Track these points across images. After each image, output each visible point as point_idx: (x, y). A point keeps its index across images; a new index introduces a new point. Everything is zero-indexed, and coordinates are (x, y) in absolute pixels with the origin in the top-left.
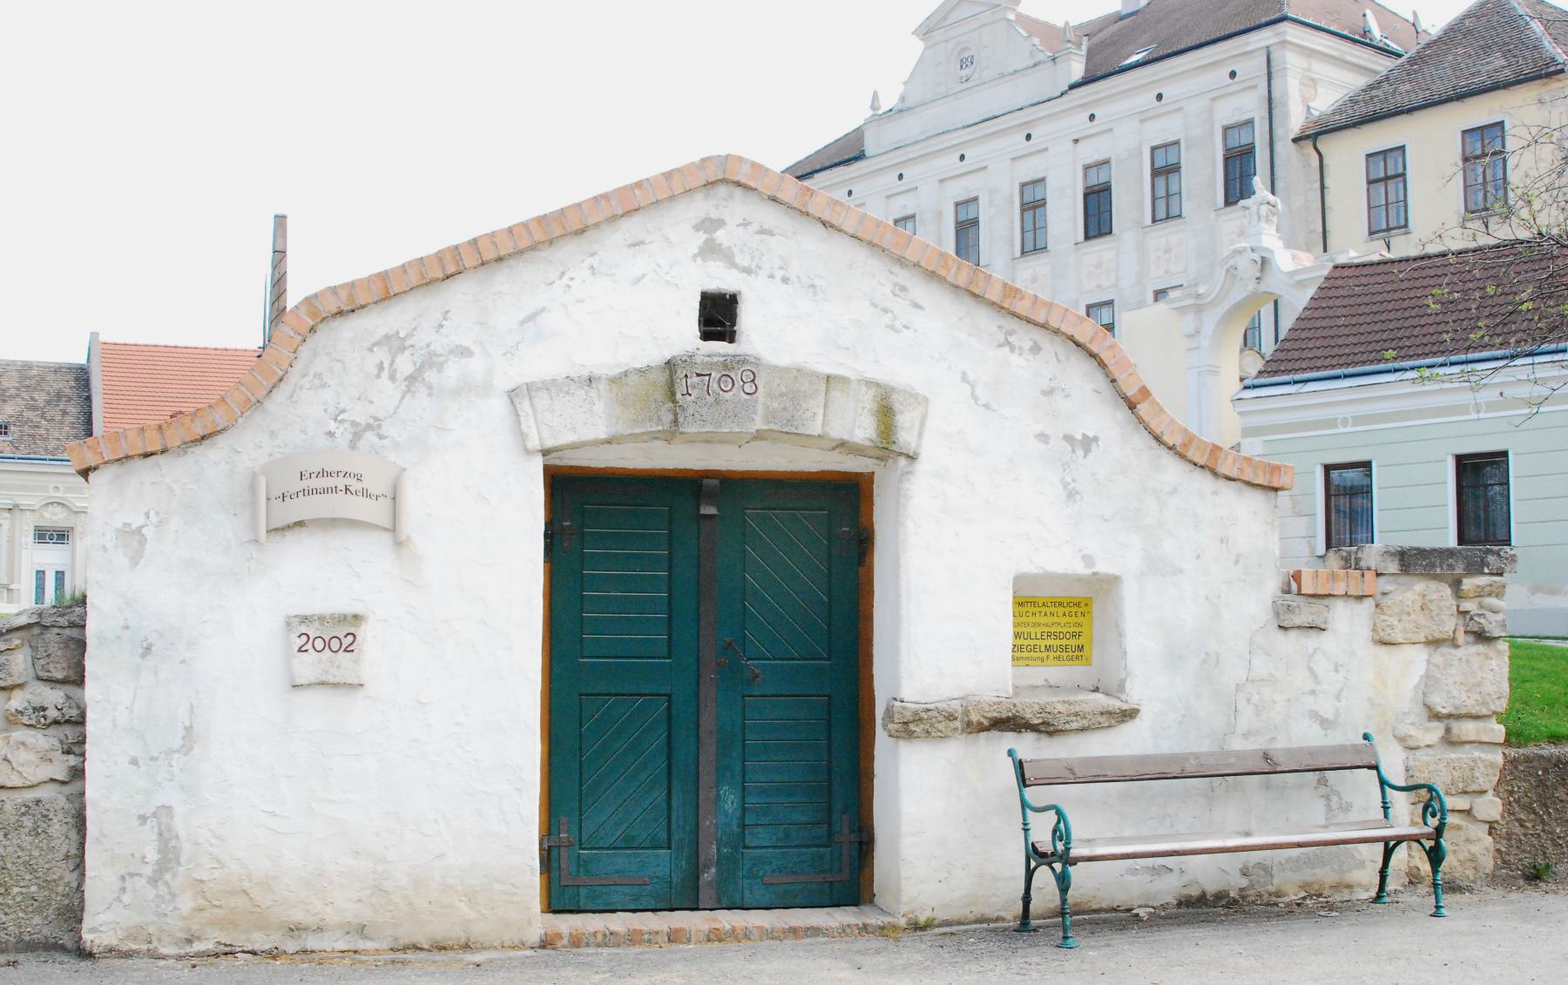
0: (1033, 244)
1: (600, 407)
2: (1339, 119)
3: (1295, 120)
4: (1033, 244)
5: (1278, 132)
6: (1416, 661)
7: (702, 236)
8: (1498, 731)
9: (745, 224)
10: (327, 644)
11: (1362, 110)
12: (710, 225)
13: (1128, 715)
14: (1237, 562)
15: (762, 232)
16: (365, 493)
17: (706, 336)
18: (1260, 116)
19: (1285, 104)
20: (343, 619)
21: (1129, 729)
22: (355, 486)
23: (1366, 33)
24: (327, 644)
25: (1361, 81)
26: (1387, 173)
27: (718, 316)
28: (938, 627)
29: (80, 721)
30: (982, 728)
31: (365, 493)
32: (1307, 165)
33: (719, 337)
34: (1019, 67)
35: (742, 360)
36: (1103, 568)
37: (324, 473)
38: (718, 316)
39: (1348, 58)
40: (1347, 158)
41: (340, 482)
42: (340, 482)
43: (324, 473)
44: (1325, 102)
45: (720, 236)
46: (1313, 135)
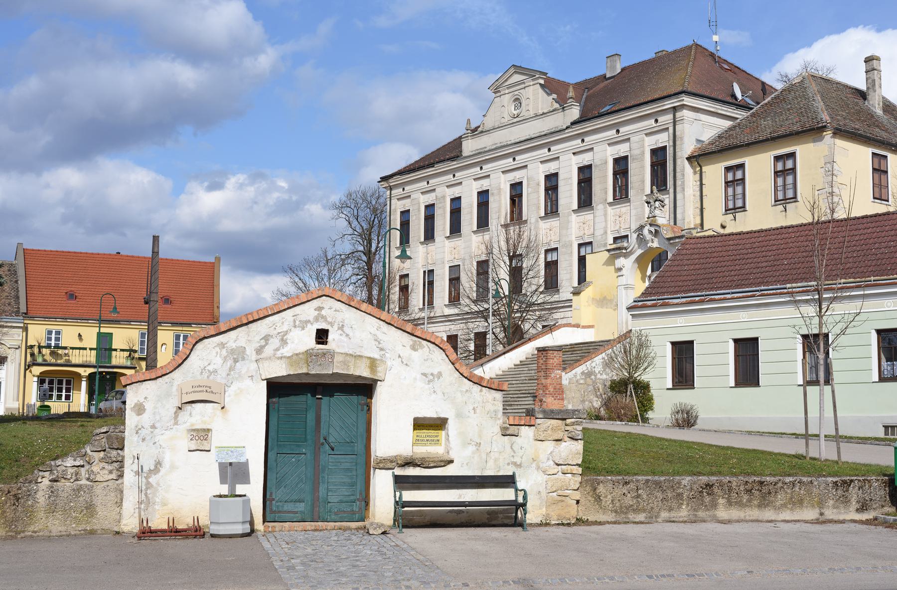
0: (552, 209)
1: (284, 366)
2: (714, 148)
3: (688, 147)
4: (552, 209)
5: (678, 154)
6: (549, 446)
7: (317, 312)
8: (580, 470)
9: (330, 308)
10: (199, 438)
11: (725, 143)
12: (320, 309)
13: (451, 462)
14: (420, 424)
15: (336, 311)
16: (212, 392)
17: (318, 343)
18: (669, 145)
19: (682, 138)
20: (204, 430)
21: (451, 466)
22: (209, 390)
23: (734, 96)
24: (199, 438)
25: (728, 124)
26: (735, 180)
27: (322, 336)
28: (391, 432)
29: (122, 462)
30: (403, 466)
31: (212, 392)
32: (695, 173)
33: (322, 343)
34: (545, 111)
35: (329, 351)
36: (442, 416)
37: (199, 386)
38: (322, 336)
39: (720, 112)
40: (715, 172)
41: (205, 389)
42: (205, 389)
43: (199, 386)
44: (708, 135)
45: (323, 312)
46: (698, 158)
